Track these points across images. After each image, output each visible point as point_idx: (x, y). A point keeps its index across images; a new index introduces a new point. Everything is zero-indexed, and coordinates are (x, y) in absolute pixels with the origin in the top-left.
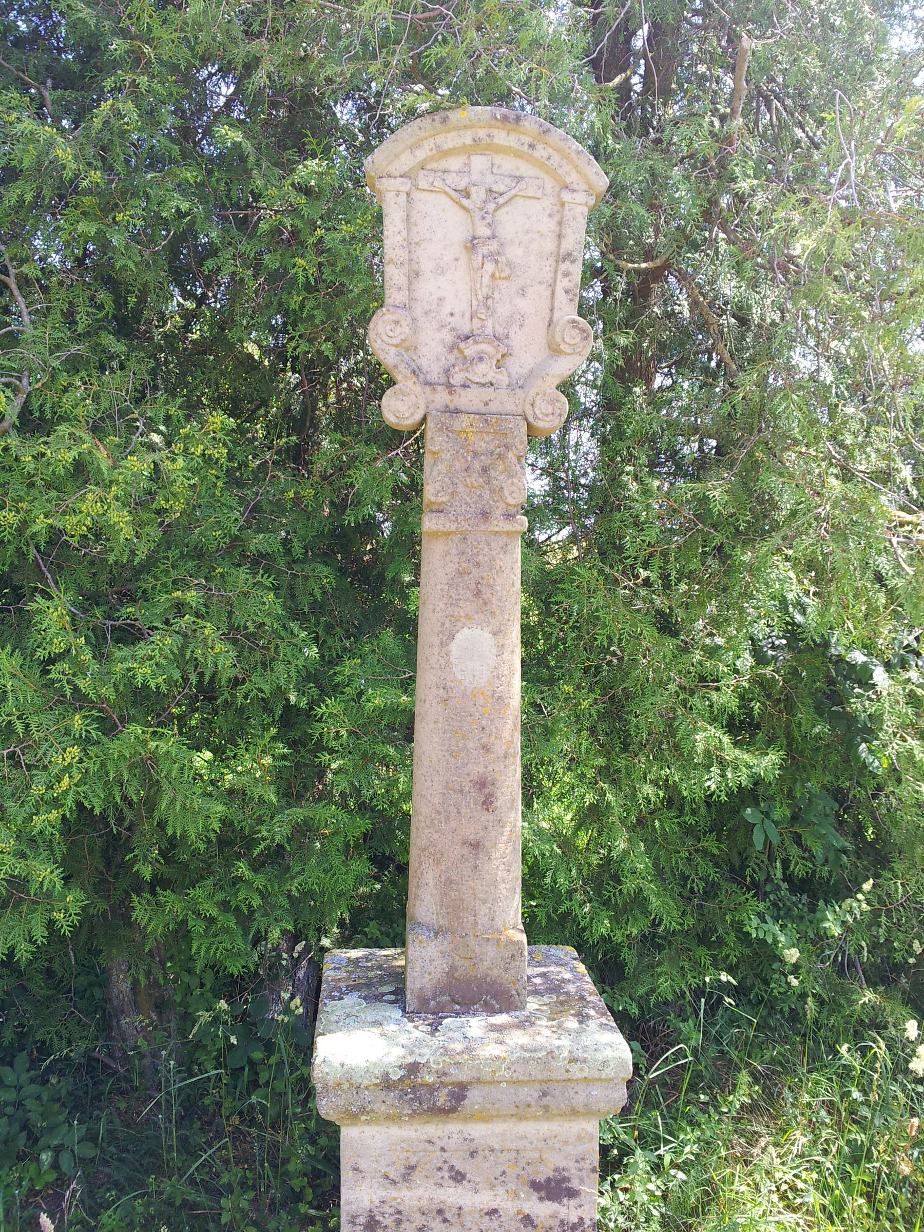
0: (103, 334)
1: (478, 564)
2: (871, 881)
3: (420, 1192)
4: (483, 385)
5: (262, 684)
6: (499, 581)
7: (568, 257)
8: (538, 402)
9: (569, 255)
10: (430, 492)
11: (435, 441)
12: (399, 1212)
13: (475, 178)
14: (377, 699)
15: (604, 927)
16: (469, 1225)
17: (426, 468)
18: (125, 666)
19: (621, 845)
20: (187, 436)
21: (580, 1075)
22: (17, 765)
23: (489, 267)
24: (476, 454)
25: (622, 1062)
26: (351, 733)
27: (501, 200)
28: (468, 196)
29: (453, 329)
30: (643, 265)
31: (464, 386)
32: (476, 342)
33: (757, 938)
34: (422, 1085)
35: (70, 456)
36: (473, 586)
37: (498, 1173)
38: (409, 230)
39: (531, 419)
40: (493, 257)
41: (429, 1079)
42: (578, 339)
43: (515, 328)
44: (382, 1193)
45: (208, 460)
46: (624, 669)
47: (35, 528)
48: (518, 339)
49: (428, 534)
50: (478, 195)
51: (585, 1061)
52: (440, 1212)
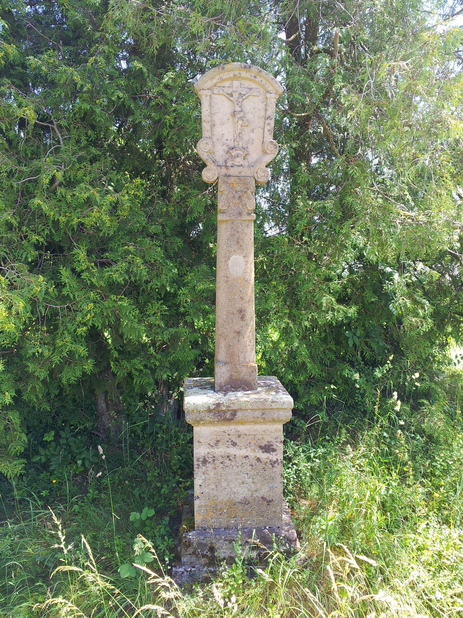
0: (91, 147)
1: (238, 232)
2: (392, 356)
3: (221, 449)
4: (239, 166)
5: (156, 283)
6: (245, 238)
7: (269, 118)
8: (259, 172)
9: (269, 117)
10: (221, 206)
11: (222, 187)
12: (214, 457)
13: (235, 89)
14: (201, 287)
15: (290, 377)
16: (238, 461)
17: (219, 197)
18: (109, 273)
19: (296, 344)
20: (128, 187)
21: (275, 407)
22: (70, 310)
23: (240, 122)
24: (236, 192)
25: (290, 403)
26: (192, 301)
27: (244, 97)
28: (232, 96)
29: (227, 145)
30: (303, 114)
31: (232, 166)
32: (236, 150)
33: (348, 377)
34: (221, 411)
35: (86, 196)
36: (236, 240)
37: (248, 443)
38: (211, 109)
39: (256, 178)
40: (242, 118)
41: (224, 408)
42: (273, 148)
43: (250, 144)
44: (208, 450)
45: (136, 196)
46: (296, 275)
47: (74, 223)
48: (251, 149)
49: (220, 221)
50: (236, 95)
51: (277, 402)
52: (228, 457)
